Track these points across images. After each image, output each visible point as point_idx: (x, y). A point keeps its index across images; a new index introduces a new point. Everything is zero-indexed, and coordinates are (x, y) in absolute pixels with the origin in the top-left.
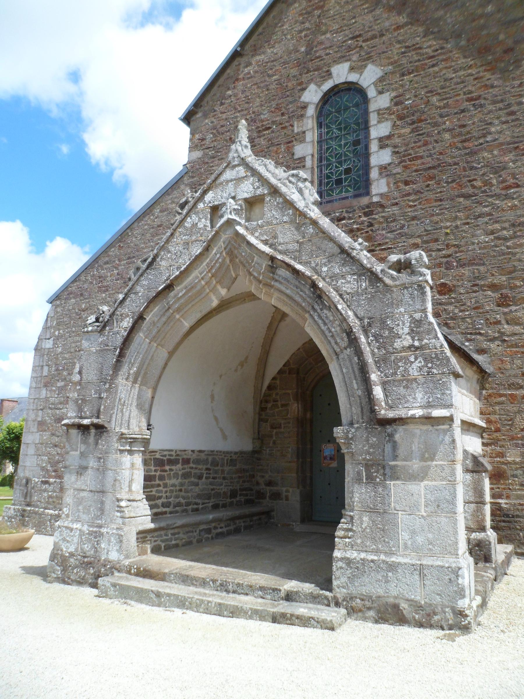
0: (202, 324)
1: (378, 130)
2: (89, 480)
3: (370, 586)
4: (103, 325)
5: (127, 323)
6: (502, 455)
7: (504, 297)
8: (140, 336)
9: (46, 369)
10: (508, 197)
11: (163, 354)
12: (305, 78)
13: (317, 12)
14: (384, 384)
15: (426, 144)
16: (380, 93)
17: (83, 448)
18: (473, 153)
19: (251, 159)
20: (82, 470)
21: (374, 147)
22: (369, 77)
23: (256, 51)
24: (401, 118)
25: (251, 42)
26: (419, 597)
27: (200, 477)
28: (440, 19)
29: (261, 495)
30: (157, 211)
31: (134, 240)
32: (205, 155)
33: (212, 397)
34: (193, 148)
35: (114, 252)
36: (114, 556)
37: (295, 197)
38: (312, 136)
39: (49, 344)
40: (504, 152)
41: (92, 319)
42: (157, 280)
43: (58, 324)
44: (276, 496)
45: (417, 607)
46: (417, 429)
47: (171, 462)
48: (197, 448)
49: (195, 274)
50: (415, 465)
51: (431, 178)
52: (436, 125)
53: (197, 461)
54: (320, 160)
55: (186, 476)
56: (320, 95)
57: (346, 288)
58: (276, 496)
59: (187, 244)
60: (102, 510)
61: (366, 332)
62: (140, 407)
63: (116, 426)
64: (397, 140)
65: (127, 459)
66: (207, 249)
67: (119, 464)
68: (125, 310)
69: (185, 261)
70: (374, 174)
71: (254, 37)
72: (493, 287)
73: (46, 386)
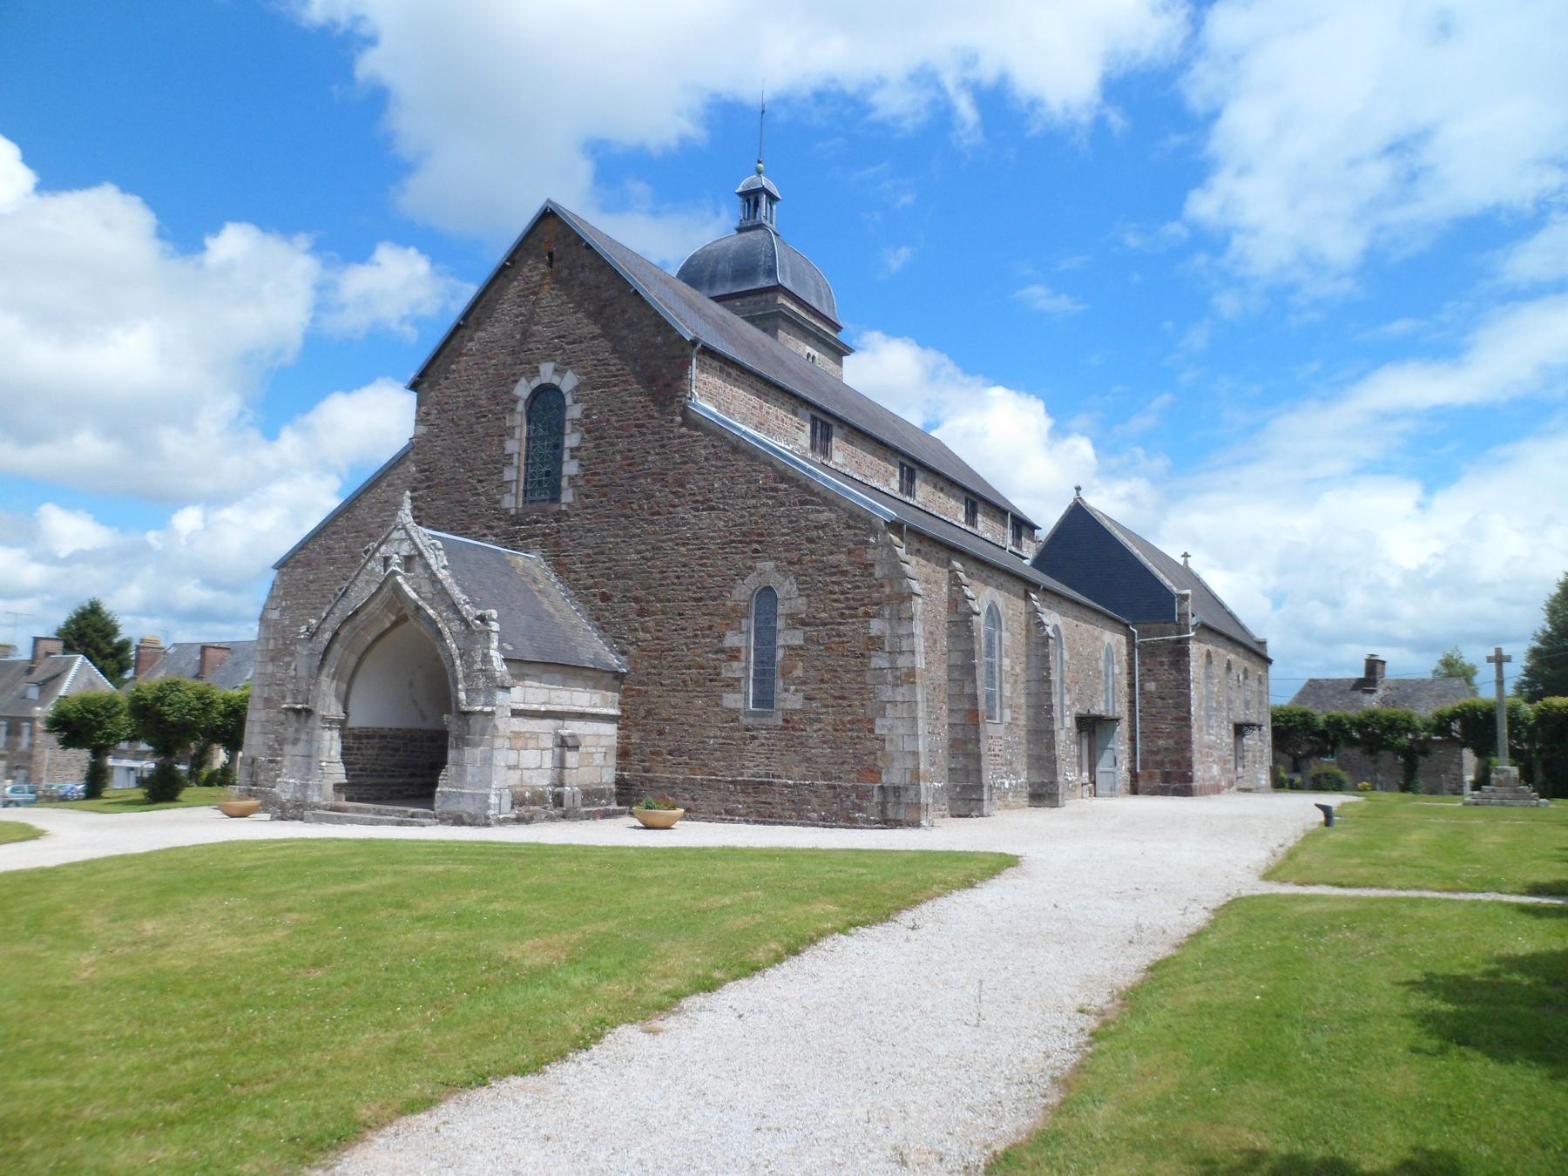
1: (571, 440)
2: (300, 749)
3: (452, 807)
4: (313, 635)
5: (328, 636)
6: (628, 737)
7: (642, 609)
8: (337, 647)
9: (272, 642)
10: (653, 523)
11: (353, 659)
12: (518, 369)
13: (533, 298)
14: (467, 691)
15: (604, 462)
16: (575, 402)
17: (296, 725)
18: (634, 478)
20: (296, 741)
22: (568, 383)
23: (479, 325)
24: (588, 431)
25: (475, 314)
26: (472, 810)
27: (397, 750)
28: (624, 338)
30: (384, 484)
31: (362, 512)
32: (430, 432)
33: (411, 684)
34: (419, 421)
35: (341, 522)
36: (316, 799)
37: (432, 561)
38: (522, 432)
39: (275, 615)
40: (655, 481)
41: (303, 629)
42: (345, 608)
43: (285, 594)
45: (470, 815)
46: (480, 718)
47: (368, 737)
48: (394, 725)
49: (372, 605)
50: (477, 738)
51: (605, 495)
52: (612, 444)
53: (394, 737)
54: (527, 457)
55: (381, 748)
56: (529, 391)
57: (454, 629)
59: (368, 582)
60: (309, 769)
61: (461, 657)
62: (337, 696)
63: (320, 711)
64: (583, 453)
65: (327, 734)
66: (380, 588)
67: (321, 736)
68: (326, 626)
69: (366, 595)
70: (565, 483)
71: (478, 309)
72: (637, 600)
73: (272, 660)
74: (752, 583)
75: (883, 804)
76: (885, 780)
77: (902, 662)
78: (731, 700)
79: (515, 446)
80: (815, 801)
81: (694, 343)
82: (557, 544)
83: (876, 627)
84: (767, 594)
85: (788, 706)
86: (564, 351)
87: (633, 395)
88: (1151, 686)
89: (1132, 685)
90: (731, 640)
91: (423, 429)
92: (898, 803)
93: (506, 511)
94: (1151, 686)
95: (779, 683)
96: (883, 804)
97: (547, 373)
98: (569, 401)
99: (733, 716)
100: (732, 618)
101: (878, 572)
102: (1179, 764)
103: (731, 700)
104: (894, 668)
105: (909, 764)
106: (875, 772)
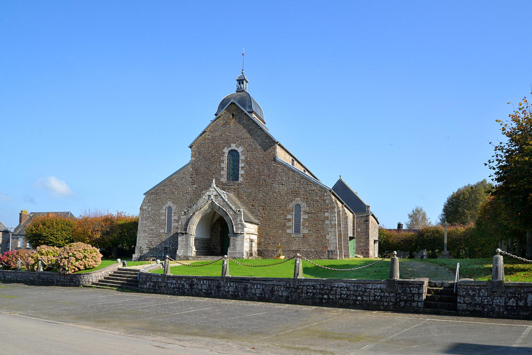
0: (270, 278)
1: (241, 165)
19: (216, 187)
21: (240, 169)
22: (240, 150)
29: (211, 248)
34: (192, 156)
44: (215, 248)
58: (215, 248)
70: (240, 176)
74: (294, 203)
75: (328, 255)
76: (329, 249)
77: (333, 222)
78: (289, 231)
79: (224, 165)
80: (311, 254)
81: (277, 143)
82: (238, 191)
83: (326, 214)
84: (298, 206)
85: (304, 232)
86: (241, 142)
87: (260, 154)
88: (359, 230)
89: (354, 229)
90: (289, 217)
91: (194, 159)
92: (332, 254)
93: (222, 182)
94: (359, 230)
95: (302, 227)
96: (328, 255)
97: (233, 147)
98: (240, 154)
99: (290, 235)
100: (289, 212)
101: (327, 202)
102: (366, 250)
103: (289, 231)
104: (331, 224)
105: (335, 245)
106: (326, 247)
